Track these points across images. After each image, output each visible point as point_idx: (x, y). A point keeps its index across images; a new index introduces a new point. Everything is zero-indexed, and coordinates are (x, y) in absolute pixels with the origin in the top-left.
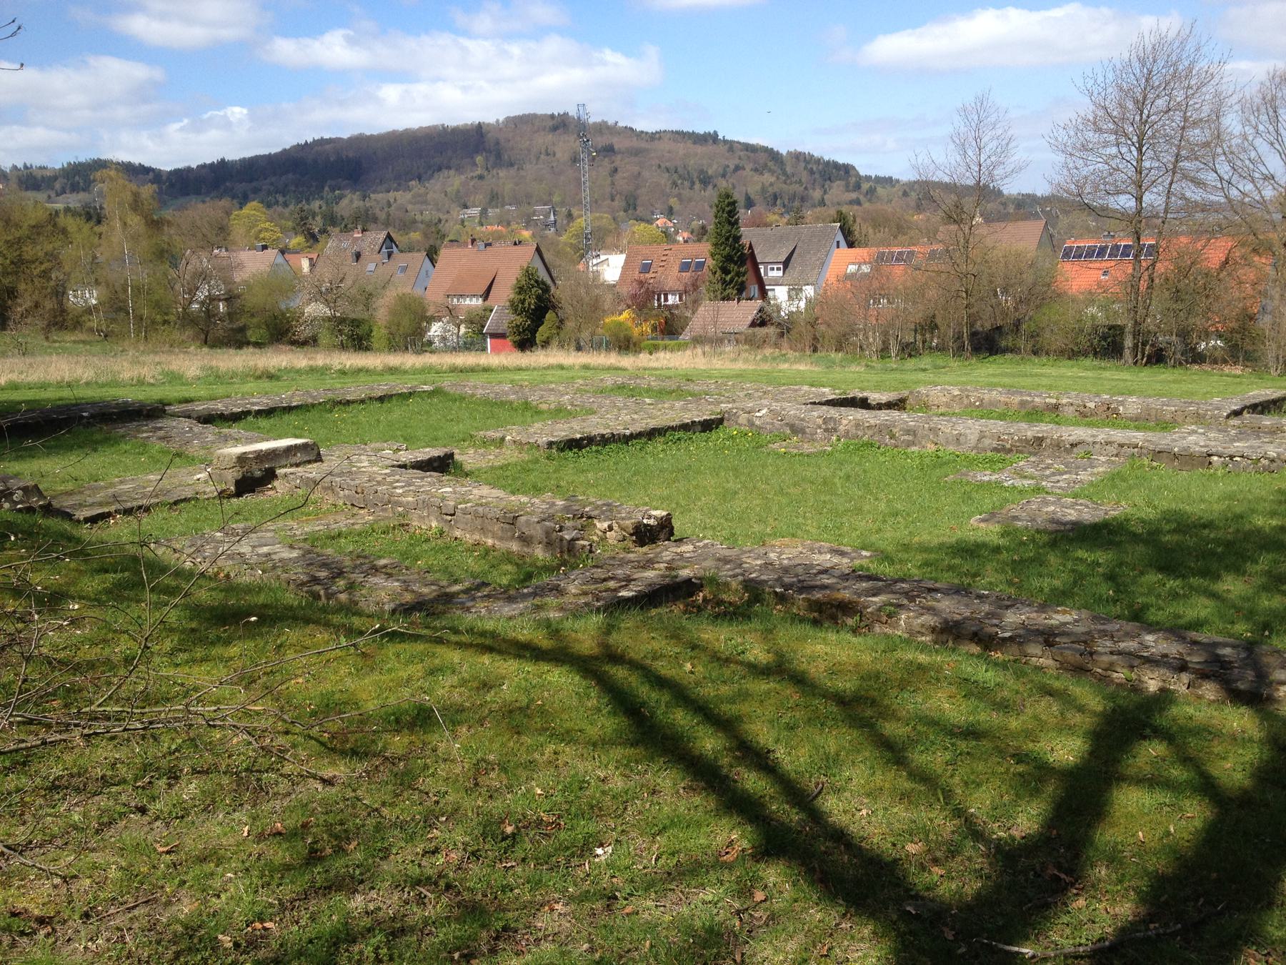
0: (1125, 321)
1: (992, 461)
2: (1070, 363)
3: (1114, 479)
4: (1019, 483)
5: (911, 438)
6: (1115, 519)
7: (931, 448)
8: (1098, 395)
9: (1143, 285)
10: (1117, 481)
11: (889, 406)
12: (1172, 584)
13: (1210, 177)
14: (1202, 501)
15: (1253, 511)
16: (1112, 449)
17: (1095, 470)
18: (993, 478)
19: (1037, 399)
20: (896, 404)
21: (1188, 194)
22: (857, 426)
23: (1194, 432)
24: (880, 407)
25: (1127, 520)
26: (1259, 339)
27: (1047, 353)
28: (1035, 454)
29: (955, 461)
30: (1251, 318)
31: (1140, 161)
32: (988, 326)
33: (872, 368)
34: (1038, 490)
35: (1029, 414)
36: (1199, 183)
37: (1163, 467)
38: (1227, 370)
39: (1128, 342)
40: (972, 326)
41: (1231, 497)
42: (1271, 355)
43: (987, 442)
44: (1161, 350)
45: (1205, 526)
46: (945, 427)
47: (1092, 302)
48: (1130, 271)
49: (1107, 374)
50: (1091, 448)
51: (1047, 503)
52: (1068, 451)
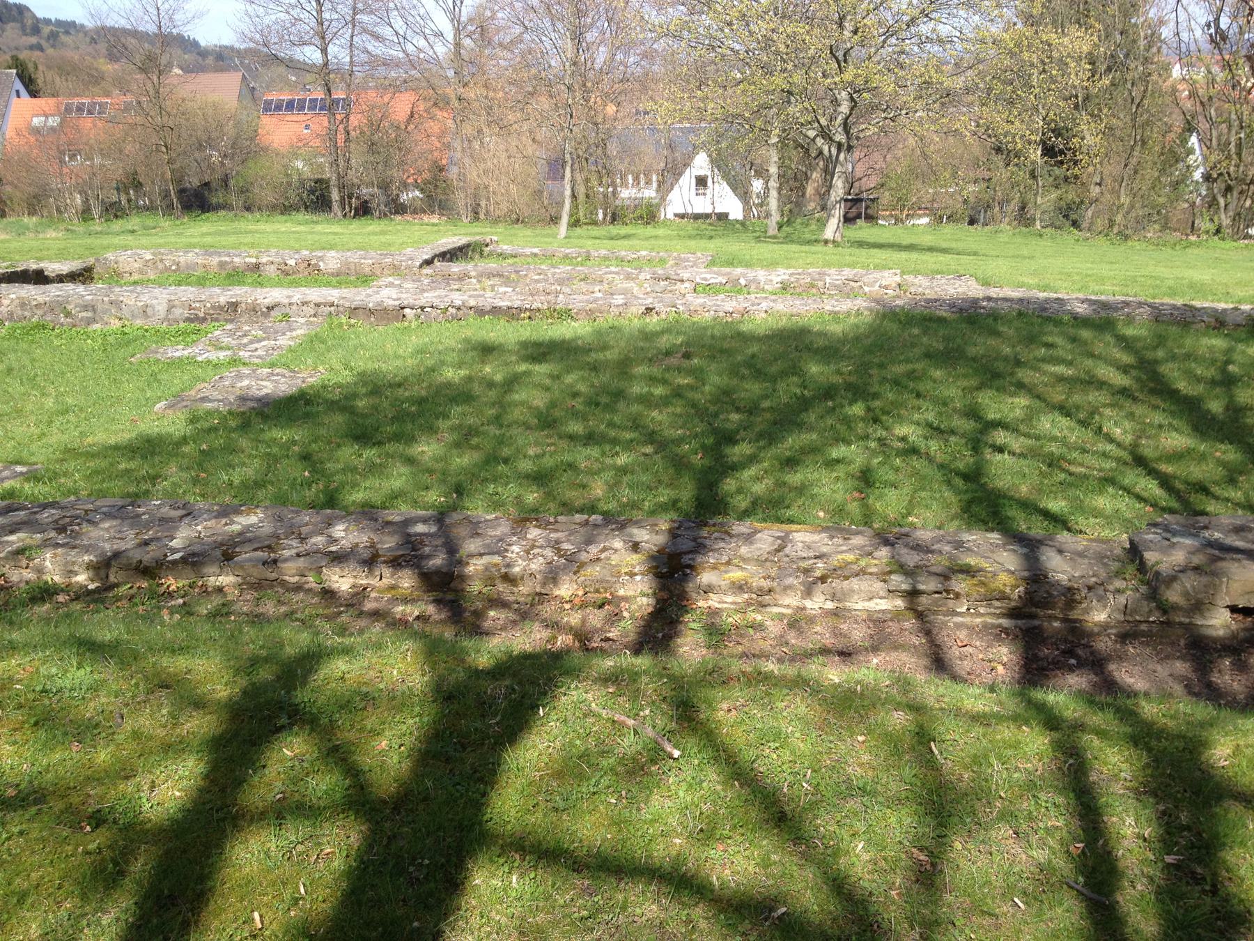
0: (328, 174)
1: (185, 333)
2: (284, 218)
3: (313, 343)
4: (215, 355)
5: (90, 314)
6: (312, 387)
7: (115, 324)
8: (298, 252)
9: (341, 137)
10: (316, 345)
11: (73, 277)
12: (370, 453)
13: (387, 32)
14: (397, 357)
15: (443, 363)
16: (309, 310)
17: (294, 334)
18: (186, 353)
19: (236, 260)
20: (80, 275)
21: (370, 48)
22: (23, 305)
23: (391, 285)
24: (60, 279)
25: (324, 387)
26: (449, 188)
27: (259, 209)
28: (231, 321)
29: (144, 336)
30: (441, 170)
31: (320, 12)
32: (196, 182)
33: (72, 231)
34: (234, 362)
35: (229, 276)
36: (376, 37)
37: (361, 324)
38: (426, 219)
39: (335, 195)
40: (180, 181)
41: (421, 351)
42: (461, 203)
43: (178, 312)
44: (366, 202)
45: (399, 385)
46: (129, 298)
47: (296, 156)
48: (326, 124)
49: (319, 228)
50: (288, 310)
51: (240, 377)
52: (266, 315)
